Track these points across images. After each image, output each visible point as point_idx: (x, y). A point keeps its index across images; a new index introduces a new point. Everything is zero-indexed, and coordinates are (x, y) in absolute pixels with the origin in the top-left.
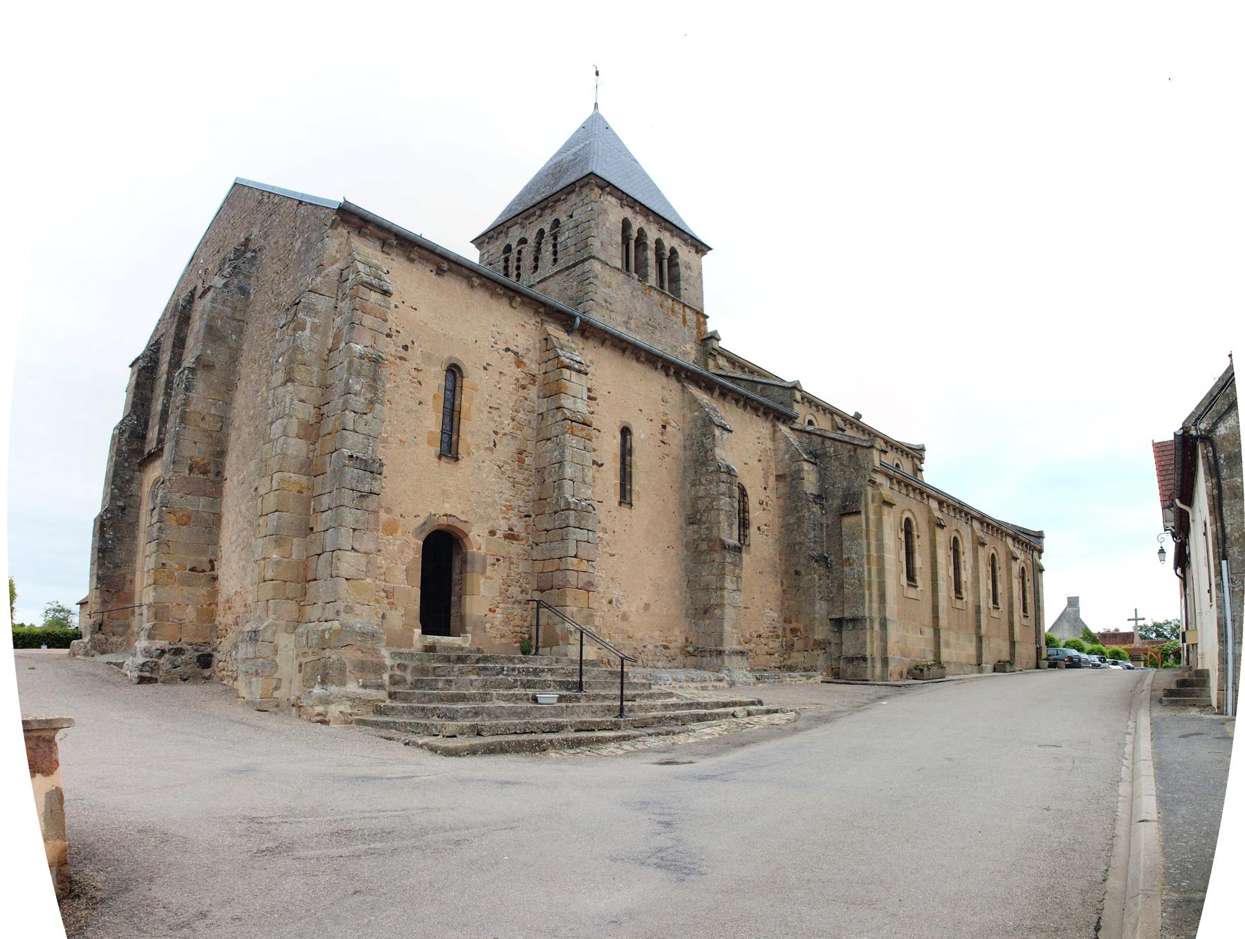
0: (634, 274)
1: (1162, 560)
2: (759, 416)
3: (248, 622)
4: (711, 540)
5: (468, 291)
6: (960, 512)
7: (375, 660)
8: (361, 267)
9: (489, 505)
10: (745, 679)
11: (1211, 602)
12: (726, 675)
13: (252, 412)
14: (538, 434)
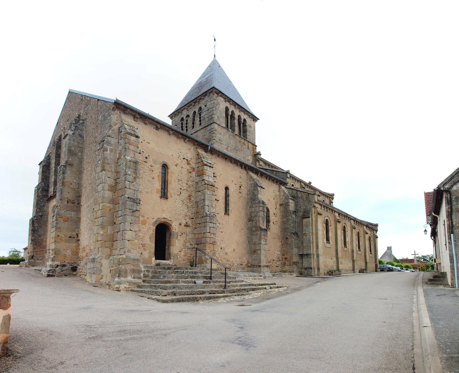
0: (230, 129)
2: (274, 183)
3: (91, 255)
4: (256, 227)
5: (168, 136)
6: (346, 217)
7: (138, 269)
8: (126, 126)
9: (179, 215)
10: (269, 275)
11: (446, 248)
12: (263, 274)
13: (90, 181)
14: (196, 190)
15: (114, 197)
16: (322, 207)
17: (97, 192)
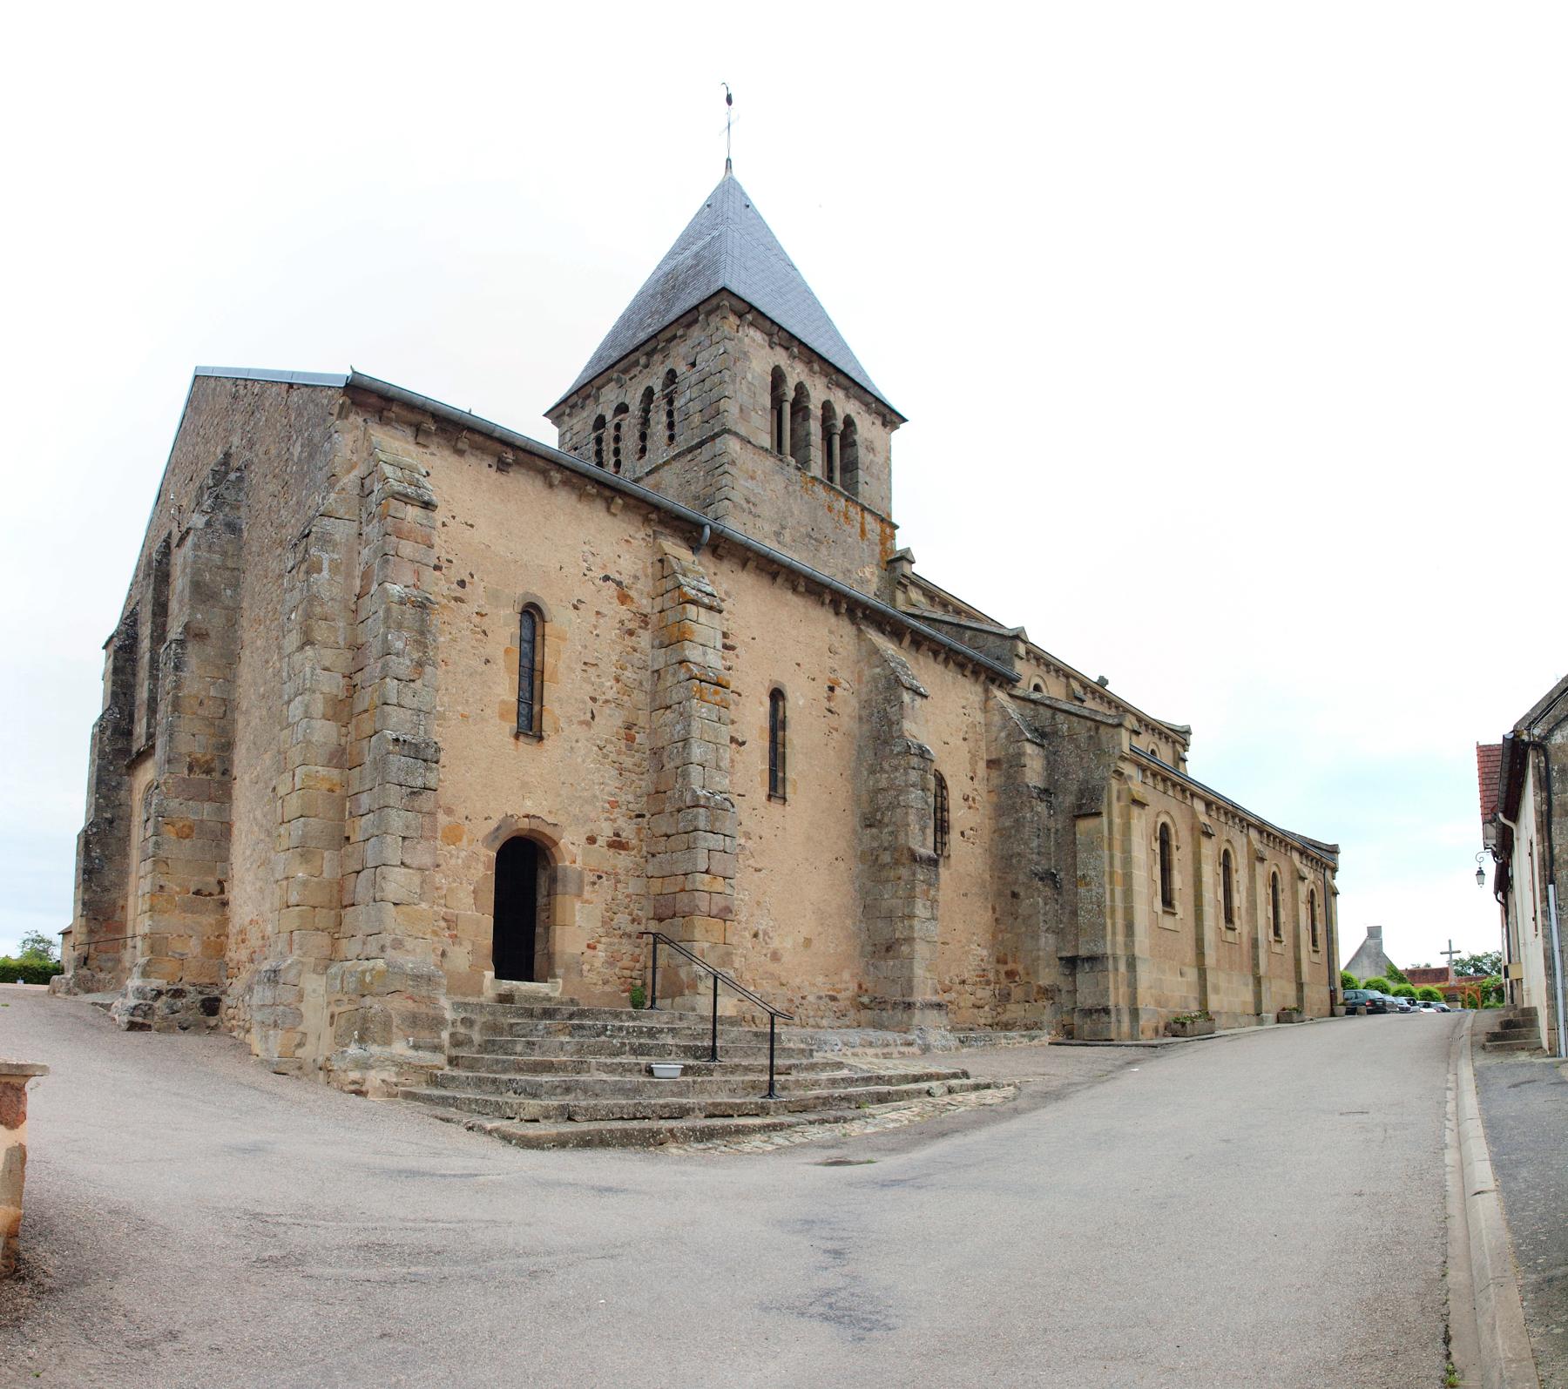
0: (789, 458)
1: (1481, 883)
5: (545, 492)
6: (1233, 817)
7: (432, 1012)
8: (388, 470)
9: (586, 802)
10: (944, 1042)
14: (653, 700)
15: (343, 741)
16: (1147, 777)
17: (285, 724)
